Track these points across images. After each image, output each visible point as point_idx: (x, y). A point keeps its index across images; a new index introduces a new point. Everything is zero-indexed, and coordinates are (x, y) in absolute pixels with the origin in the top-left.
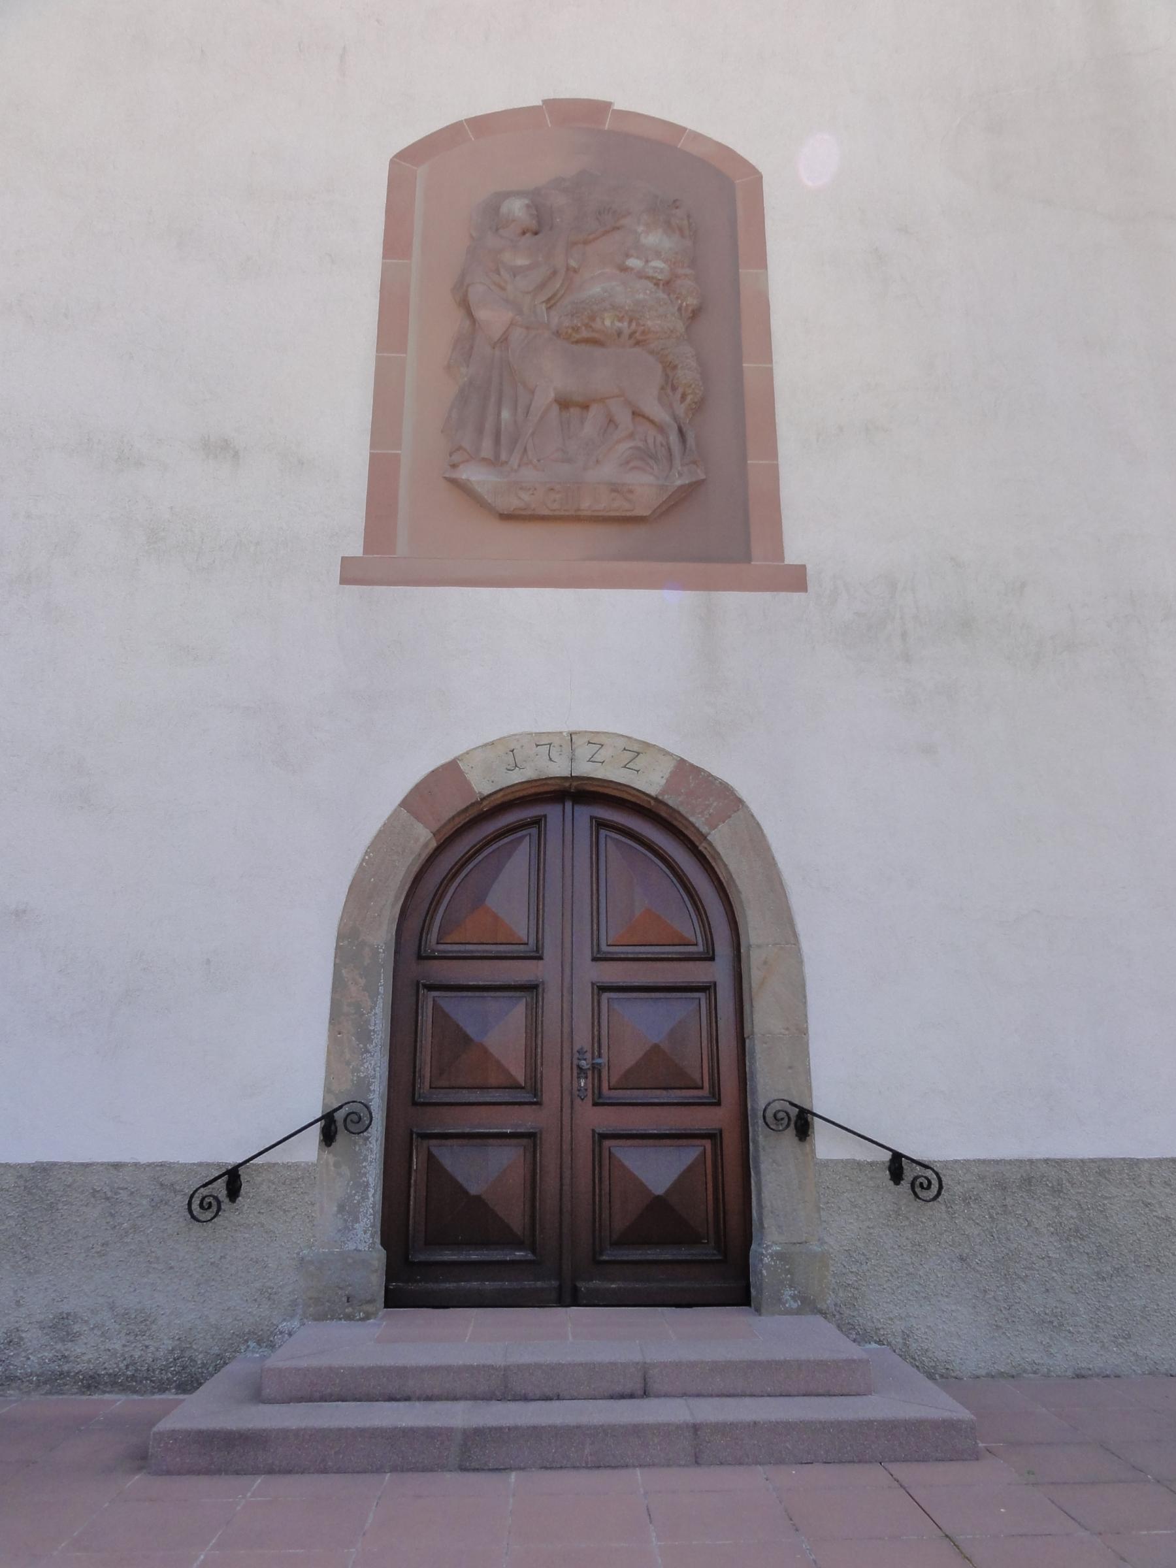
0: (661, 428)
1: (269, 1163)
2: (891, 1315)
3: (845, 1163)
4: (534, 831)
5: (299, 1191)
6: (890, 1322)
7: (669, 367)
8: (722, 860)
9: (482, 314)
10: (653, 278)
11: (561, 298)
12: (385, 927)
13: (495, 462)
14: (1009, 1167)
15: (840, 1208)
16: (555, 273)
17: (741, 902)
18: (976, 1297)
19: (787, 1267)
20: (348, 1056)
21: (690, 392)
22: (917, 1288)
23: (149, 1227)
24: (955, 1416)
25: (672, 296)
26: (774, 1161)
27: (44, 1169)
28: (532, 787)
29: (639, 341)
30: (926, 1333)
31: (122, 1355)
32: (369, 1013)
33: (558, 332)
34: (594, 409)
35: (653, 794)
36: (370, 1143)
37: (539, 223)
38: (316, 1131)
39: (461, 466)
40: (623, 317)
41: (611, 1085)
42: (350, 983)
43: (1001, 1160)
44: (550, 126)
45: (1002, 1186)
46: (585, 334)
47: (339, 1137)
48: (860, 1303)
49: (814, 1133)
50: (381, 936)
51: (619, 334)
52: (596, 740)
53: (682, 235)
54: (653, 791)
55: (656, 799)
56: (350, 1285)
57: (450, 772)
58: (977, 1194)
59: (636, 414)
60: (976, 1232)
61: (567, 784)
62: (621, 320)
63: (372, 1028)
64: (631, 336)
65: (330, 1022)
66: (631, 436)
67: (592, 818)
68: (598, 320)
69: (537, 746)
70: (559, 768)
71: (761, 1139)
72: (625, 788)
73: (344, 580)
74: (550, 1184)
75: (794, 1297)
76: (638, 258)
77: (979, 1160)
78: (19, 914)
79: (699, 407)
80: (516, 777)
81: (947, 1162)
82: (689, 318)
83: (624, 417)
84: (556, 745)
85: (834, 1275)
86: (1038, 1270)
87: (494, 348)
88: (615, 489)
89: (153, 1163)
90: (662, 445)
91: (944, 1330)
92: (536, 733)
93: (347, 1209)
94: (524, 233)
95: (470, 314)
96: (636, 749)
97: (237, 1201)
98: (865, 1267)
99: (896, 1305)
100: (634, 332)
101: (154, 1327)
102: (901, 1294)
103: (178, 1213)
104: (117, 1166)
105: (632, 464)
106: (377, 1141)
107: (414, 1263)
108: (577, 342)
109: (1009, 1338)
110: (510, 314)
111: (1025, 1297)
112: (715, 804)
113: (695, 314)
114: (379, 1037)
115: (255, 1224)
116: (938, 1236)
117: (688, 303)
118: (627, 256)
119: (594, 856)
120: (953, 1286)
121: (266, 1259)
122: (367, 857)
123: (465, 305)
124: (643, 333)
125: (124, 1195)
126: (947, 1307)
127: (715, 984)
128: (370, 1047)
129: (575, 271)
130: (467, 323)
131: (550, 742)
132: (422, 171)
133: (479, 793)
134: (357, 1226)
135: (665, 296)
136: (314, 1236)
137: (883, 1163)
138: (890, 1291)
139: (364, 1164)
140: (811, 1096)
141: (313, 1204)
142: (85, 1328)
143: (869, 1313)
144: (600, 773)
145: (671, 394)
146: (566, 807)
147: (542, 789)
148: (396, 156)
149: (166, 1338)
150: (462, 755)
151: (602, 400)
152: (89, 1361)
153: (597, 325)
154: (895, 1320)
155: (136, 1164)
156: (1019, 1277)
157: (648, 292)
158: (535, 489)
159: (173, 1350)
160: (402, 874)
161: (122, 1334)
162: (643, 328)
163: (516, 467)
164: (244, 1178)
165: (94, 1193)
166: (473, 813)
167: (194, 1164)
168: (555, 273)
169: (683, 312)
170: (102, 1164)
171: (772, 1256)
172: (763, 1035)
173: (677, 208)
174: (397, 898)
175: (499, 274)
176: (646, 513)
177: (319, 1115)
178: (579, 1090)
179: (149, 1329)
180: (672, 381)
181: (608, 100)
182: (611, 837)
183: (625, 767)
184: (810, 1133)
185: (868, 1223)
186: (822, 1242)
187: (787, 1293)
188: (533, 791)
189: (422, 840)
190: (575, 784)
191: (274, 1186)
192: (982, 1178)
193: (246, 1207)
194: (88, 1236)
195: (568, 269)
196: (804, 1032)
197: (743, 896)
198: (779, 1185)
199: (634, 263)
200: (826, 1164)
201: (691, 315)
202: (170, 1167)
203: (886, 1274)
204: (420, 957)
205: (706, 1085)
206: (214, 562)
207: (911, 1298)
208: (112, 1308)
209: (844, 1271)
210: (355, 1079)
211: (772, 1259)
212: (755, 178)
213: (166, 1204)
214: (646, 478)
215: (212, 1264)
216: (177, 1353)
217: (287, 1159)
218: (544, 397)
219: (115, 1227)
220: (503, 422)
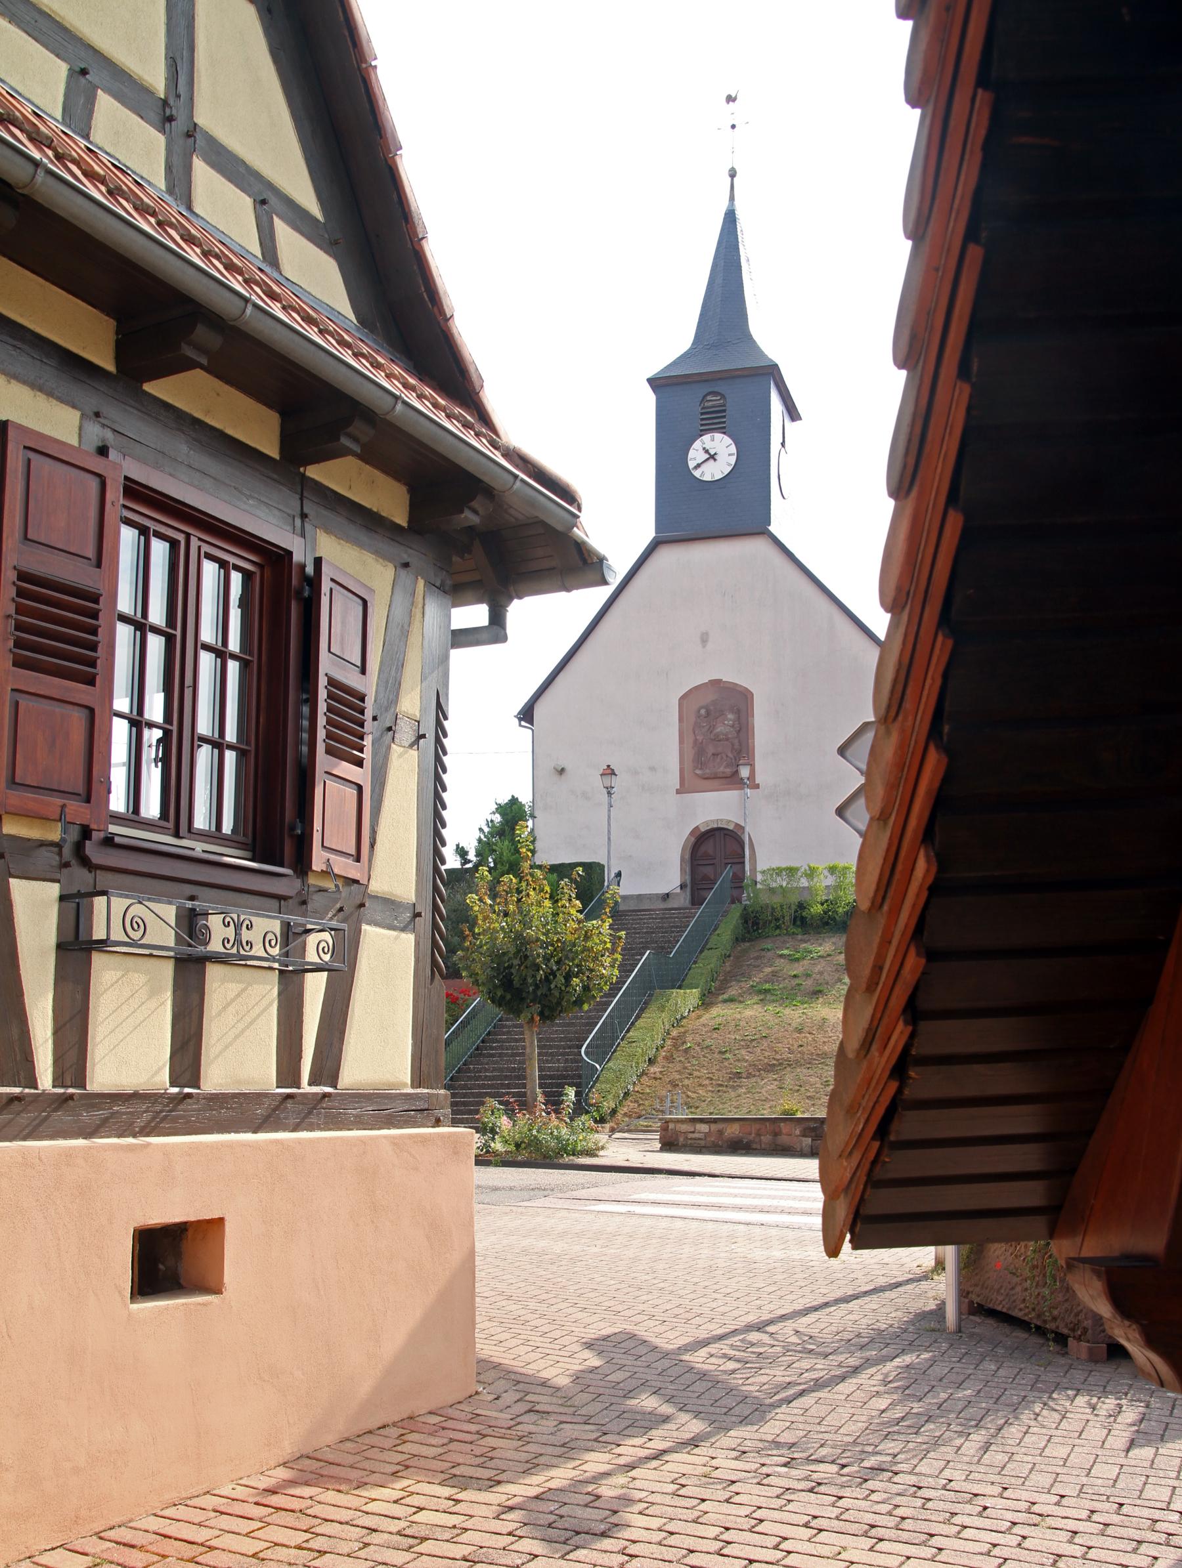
13: (701, 769)
24: (289, 230)
27: (640, 895)
29: (727, 739)
50: (687, 856)
57: (697, 827)
73: (677, 793)
78: (630, 856)
83: (725, 758)
93: (685, 899)
199: (726, 722)
212: (752, 695)
218: (710, 754)
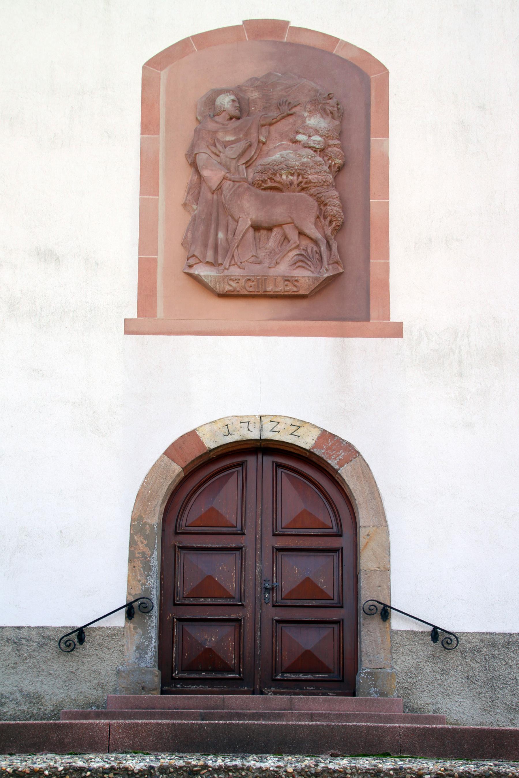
0: (315, 242)
1: (99, 627)
2: (428, 702)
3: (407, 632)
4: (240, 469)
5: (116, 640)
6: (427, 705)
7: (322, 203)
8: (346, 483)
9: (206, 173)
10: (313, 147)
11: (255, 160)
12: (157, 515)
14: (497, 636)
15: (403, 653)
16: (250, 146)
17: (356, 505)
18: (474, 696)
19: (373, 679)
20: (139, 578)
21: (335, 219)
22: (442, 691)
23: (37, 656)
25: (325, 158)
26: (369, 631)
28: (238, 445)
30: (446, 711)
31: (27, 712)
32: (150, 557)
33: (253, 183)
34: (275, 231)
35: (308, 448)
36: (152, 618)
37: (241, 109)
38: (123, 612)
39: (194, 266)
40: (294, 173)
41: (283, 596)
42: (139, 543)
43: (494, 633)
44: (247, 40)
45: (494, 645)
46: (270, 184)
47: (136, 616)
48: (411, 696)
49: (391, 617)
51: (291, 184)
52: (275, 420)
53: (333, 118)
54: (307, 447)
55: (309, 451)
56: (144, 682)
57: (193, 435)
58: (479, 649)
59: (301, 233)
60: (477, 666)
61: (259, 444)
62: (292, 175)
63: (152, 564)
64: (298, 185)
65: (129, 562)
66: (298, 247)
67: (273, 462)
68: (278, 175)
69: (241, 423)
70: (254, 435)
71: (362, 620)
72: (292, 446)
73: (127, 332)
74: (248, 644)
75: (376, 692)
76: (304, 134)
77: (481, 633)
79: (340, 229)
80: (229, 439)
81: (463, 633)
82: (336, 172)
83: (293, 236)
84: (252, 422)
85: (398, 683)
86: (509, 685)
87: (213, 194)
88: (287, 279)
89: (38, 627)
90: (316, 253)
91: (456, 710)
92: (240, 416)
93: (141, 649)
94: (231, 118)
95: (197, 171)
96: (298, 425)
97: (83, 644)
98: (415, 680)
99: (431, 698)
100: (301, 182)
101: (43, 700)
102: (434, 693)
103: (52, 649)
104: (19, 628)
105: (297, 265)
106: (156, 617)
107: (175, 679)
108: (265, 189)
109: (491, 715)
110: (223, 173)
111: (502, 697)
112: (343, 454)
113: (340, 169)
114: (156, 569)
115: (93, 655)
116: (455, 667)
117: (336, 162)
118: (297, 133)
119: (274, 497)
120: (462, 690)
121: (99, 670)
122: (146, 480)
123: (194, 164)
124: (306, 183)
125: (24, 641)
126: (458, 700)
127: (342, 548)
128: (151, 574)
129: (264, 144)
130: (196, 177)
131: (248, 421)
132: (164, 74)
133: (208, 448)
134: (146, 656)
135: (321, 159)
136: (124, 660)
137: (428, 632)
138: (428, 691)
139: (149, 628)
140: (390, 600)
141: (123, 646)
142: (7, 700)
143: (416, 701)
144: (277, 437)
145: (323, 221)
146: (258, 458)
147: (243, 447)
148: (146, 64)
149: (49, 705)
150: (198, 427)
151: (280, 226)
152: (11, 715)
153: (278, 178)
154: (430, 705)
155: (29, 628)
156: (499, 687)
157: (310, 157)
158: (239, 280)
159: (54, 710)
160: (166, 489)
161: (27, 703)
162: (306, 179)
163: (227, 267)
164: (86, 633)
165: (8, 640)
166: (206, 459)
167: (60, 627)
168: (250, 146)
169: (332, 168)
170: (11, 627)
171: (365, 673)
172: (365, 570)
173: (330, 99)
174: (163, 501)
175: (215, 146)
176: (307, 293)
177: (125, 604)
178: (265, 599)
179: (41, 701)
180: (324, 212)
181: (286, 19)
182: (284, 472)
183: (291, 434)
184: (389, 618)
185: (418, 660)
186: (392, 668)
187: (373, 690)
188: (239, 447)
189: (177, 472)
190: (263, 443)
191: (102, 638)
192: (482, 641)
193: (88, 647)
194: (6, 660)
195: (259, 142)
196: (388, 570)
197: (357, 502)
198: (371, 642)
199: (301, 137)
200: (397, 632)
201: (338, 169)
202: (47, 628)
203: (426, 684)
204: (176, 533)
205: (336, 598)
206: (49, 322)
207: (439, 695)
208: (21, 691)
209: (404, 681)
210: (143, 588)
211: (365, 675)
212: (386, 72)
213: (46, 645)
214: (307, 273)
215: (72, 672)
216: (55, 712)
217: (108, 625)
218: (245, 224)
219: (20, 656)
220: (219, 240)
